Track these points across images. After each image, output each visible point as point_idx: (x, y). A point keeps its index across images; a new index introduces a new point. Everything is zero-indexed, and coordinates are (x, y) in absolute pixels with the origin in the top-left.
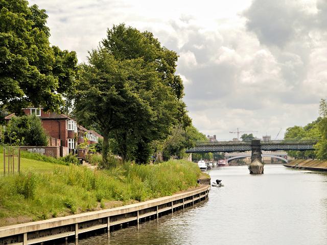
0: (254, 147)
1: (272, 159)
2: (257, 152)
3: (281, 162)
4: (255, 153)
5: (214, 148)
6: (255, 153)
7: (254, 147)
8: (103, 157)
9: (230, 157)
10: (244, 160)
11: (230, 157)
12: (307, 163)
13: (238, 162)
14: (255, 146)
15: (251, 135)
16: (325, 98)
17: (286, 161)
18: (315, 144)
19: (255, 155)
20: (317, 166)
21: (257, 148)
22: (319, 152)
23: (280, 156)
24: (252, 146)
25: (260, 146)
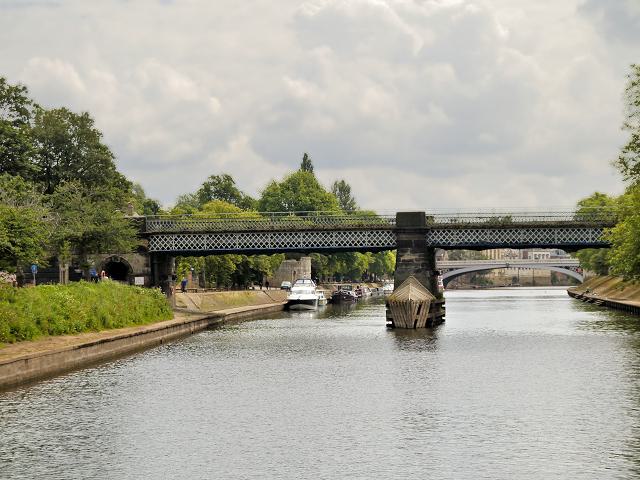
0: (404, 237)
1: (554, 275)
2: (413, 252)
3: (569, 281)
4: (407, 256)
5: (205, 242)
6: (407, 256)
7: (404, 237)
8: (307, 255)
9: (451, 270)
10: (487, 276)
11: (451, 270)
12: (615, 287)
13: (473, 280)
14: (404, 232)
15: (63, 108)
16: (638, 134)
17: (581, 279)
18: (612, 226)
19: (408, 263)
20: (633, 297)
21: (414, 238)
22: (620, 252)
23: (567, 268)
24: (396, 231)
25: (425, 232)
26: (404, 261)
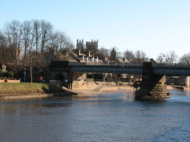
24: (142, 68)
26: (145, 78)
